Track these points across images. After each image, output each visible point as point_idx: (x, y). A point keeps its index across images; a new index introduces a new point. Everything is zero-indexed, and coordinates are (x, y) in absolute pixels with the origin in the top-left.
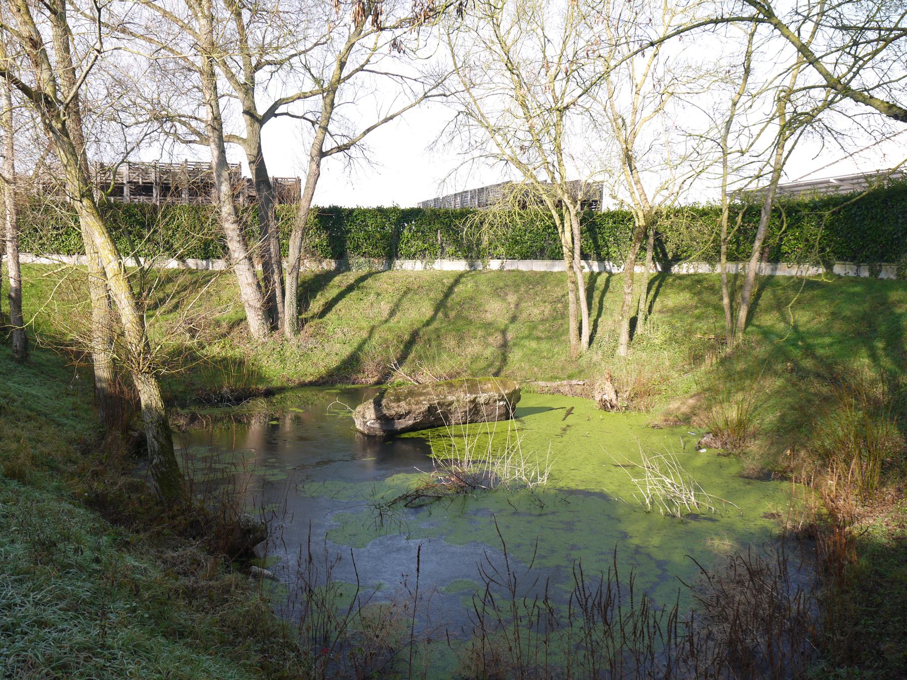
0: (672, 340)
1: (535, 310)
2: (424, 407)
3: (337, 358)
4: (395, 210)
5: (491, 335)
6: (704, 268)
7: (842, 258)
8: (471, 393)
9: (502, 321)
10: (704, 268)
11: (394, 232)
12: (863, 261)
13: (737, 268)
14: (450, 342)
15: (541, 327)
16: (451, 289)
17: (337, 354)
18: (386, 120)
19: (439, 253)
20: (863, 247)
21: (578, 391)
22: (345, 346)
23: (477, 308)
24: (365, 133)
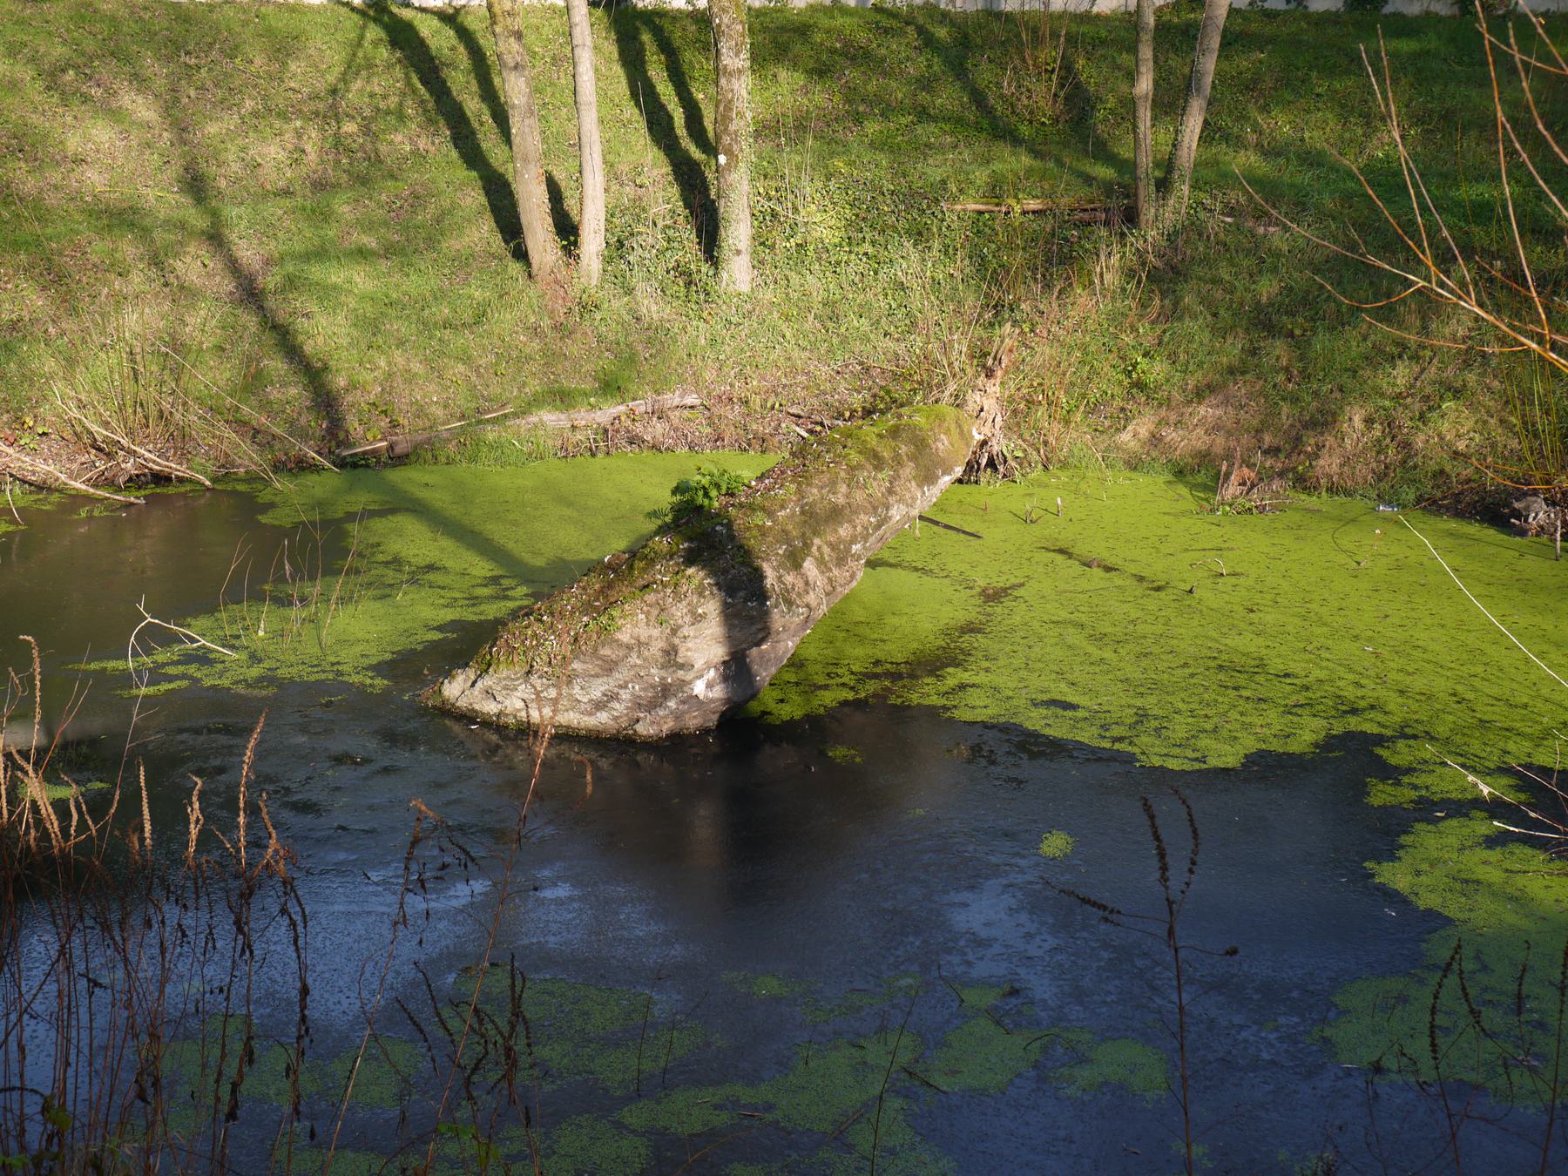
0: (865, 222)
5: (176, 250)
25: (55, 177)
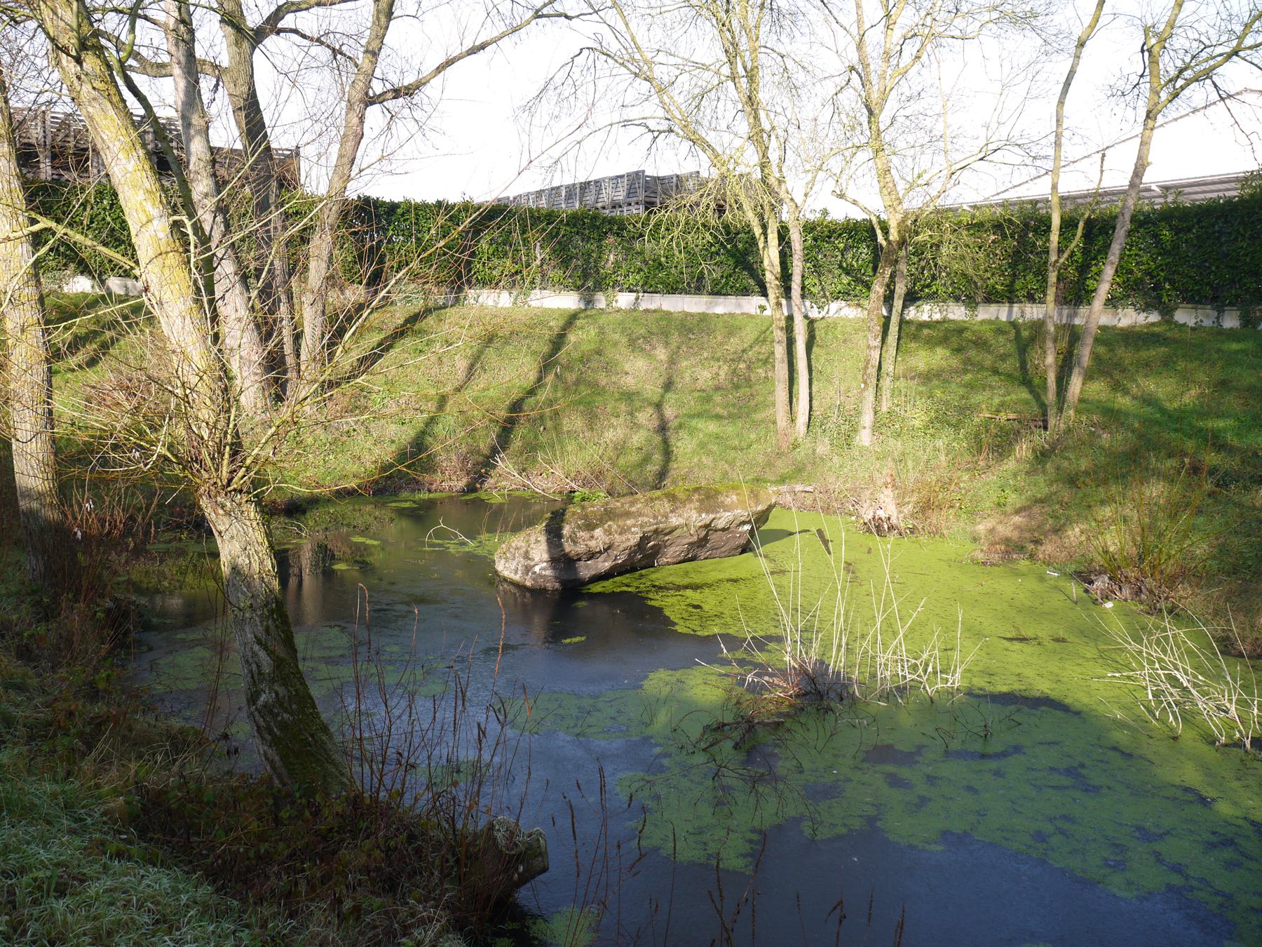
0: (940, 421)
1: (701, 373)
2: (634, 539)
3: (394, 448)
4: (467, 207)
5: (639, 409)
6: (957, 313)
7: (1194, 298)
8: (708, 512)
9: (652, 390)
10: (957, 313)
11: (478, 239)
12: (1231, 304)
13: (1010, 312)
14: (573, 422)
15: (717, 398)
16: (558, 342)
17: (393, 442)
18: (473, 51)
19: (538, 281)
20: (1233, 282)
21: (809, 502)
22: (405, 427)
23: (609, 367)
24: (440, 69)
25: (614, 379)
